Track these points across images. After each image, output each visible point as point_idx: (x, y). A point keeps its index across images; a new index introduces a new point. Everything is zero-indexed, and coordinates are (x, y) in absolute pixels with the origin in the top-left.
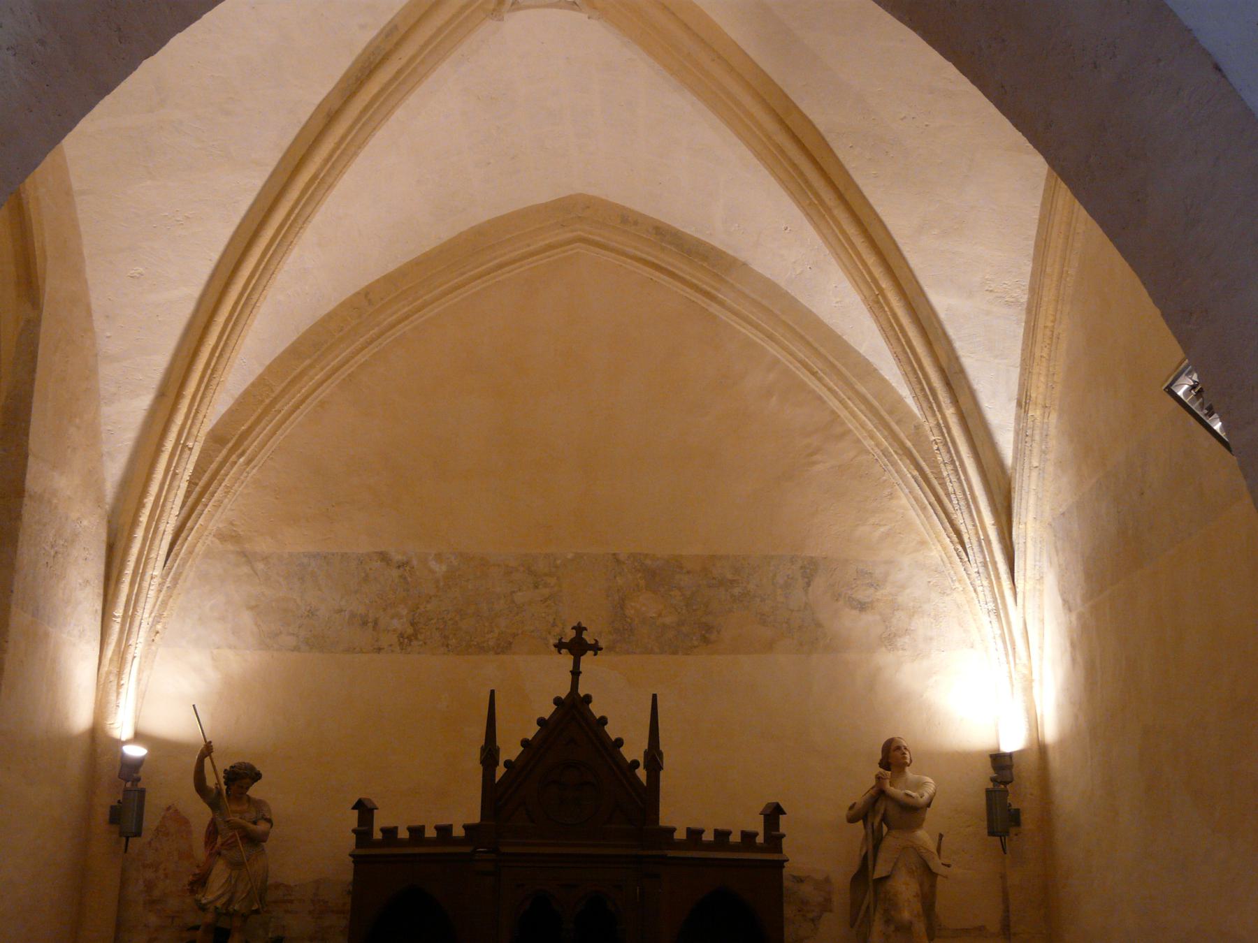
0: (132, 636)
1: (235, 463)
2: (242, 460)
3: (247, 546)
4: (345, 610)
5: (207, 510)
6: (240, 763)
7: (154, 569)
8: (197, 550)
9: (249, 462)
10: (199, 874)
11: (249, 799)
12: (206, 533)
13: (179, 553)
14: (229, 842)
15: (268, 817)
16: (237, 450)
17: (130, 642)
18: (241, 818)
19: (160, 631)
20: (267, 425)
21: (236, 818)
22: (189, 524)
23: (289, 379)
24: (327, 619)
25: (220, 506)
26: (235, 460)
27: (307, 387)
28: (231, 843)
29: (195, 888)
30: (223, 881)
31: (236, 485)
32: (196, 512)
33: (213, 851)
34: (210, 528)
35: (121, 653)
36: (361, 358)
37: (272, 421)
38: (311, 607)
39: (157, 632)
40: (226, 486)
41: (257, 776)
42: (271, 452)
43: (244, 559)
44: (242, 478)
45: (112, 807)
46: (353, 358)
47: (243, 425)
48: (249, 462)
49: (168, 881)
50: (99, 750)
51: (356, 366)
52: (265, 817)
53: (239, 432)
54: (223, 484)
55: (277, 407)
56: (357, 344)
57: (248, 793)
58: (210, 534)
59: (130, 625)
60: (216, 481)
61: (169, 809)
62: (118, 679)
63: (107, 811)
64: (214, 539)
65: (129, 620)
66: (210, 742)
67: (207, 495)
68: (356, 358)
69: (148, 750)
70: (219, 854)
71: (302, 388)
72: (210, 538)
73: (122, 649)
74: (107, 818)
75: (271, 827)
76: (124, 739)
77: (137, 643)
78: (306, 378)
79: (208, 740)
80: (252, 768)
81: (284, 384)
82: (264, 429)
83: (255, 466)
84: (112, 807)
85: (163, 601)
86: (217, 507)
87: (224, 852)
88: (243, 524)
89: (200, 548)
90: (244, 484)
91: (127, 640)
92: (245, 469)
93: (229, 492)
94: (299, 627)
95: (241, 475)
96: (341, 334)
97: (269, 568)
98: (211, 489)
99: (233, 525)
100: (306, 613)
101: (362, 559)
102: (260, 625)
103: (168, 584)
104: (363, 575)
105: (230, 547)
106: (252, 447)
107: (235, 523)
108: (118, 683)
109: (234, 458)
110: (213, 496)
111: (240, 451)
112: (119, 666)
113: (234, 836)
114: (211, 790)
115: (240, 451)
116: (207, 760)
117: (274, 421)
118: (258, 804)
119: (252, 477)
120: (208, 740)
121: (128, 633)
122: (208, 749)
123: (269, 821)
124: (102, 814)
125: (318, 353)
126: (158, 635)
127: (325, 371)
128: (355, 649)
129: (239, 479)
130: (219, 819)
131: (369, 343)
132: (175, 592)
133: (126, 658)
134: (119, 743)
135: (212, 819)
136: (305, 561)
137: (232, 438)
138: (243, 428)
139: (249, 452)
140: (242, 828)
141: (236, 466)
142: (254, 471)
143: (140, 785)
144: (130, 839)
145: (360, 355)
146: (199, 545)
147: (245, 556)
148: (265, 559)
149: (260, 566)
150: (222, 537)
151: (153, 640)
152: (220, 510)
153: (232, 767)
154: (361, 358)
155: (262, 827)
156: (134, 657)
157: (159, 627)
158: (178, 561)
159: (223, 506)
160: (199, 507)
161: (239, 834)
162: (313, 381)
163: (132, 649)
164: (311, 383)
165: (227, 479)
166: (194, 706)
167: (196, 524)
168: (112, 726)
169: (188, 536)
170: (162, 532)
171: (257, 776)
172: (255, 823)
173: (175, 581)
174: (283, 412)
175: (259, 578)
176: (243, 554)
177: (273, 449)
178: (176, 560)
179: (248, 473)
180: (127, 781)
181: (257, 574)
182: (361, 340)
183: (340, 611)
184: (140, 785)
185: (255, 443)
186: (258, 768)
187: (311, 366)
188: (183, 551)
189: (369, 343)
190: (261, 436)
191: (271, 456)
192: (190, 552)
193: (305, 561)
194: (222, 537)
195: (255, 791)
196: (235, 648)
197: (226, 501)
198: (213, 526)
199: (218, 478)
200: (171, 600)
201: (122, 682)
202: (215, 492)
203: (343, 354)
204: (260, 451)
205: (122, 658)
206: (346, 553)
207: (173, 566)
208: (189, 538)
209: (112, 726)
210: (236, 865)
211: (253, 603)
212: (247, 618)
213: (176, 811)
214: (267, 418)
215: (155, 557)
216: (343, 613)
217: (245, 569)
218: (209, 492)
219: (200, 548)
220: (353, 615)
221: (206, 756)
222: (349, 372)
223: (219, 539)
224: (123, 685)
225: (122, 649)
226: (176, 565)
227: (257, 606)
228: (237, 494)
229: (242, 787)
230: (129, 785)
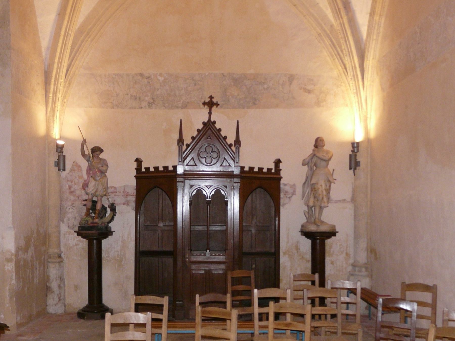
2: (89, 39)
32: (75, 59)
66: (85, 139)
67: (78, 53)
69: (65, 142)
79: (84, 138)
100: (115, 95)
103: (67, 85)
108: (53, 119)
109: (87, 39)
116: (85, 146)
120: (84, 138)
122: (85, 141)
134: (55, 140)
136: (114, 76)
151: (64, 105)
168: (52, 134)
170: (63, 65)
193: (114, 76)
195: (102, 156)
201: (54, 119)
207: (68, 78)
213: (76, 163)
215: (61, 75)
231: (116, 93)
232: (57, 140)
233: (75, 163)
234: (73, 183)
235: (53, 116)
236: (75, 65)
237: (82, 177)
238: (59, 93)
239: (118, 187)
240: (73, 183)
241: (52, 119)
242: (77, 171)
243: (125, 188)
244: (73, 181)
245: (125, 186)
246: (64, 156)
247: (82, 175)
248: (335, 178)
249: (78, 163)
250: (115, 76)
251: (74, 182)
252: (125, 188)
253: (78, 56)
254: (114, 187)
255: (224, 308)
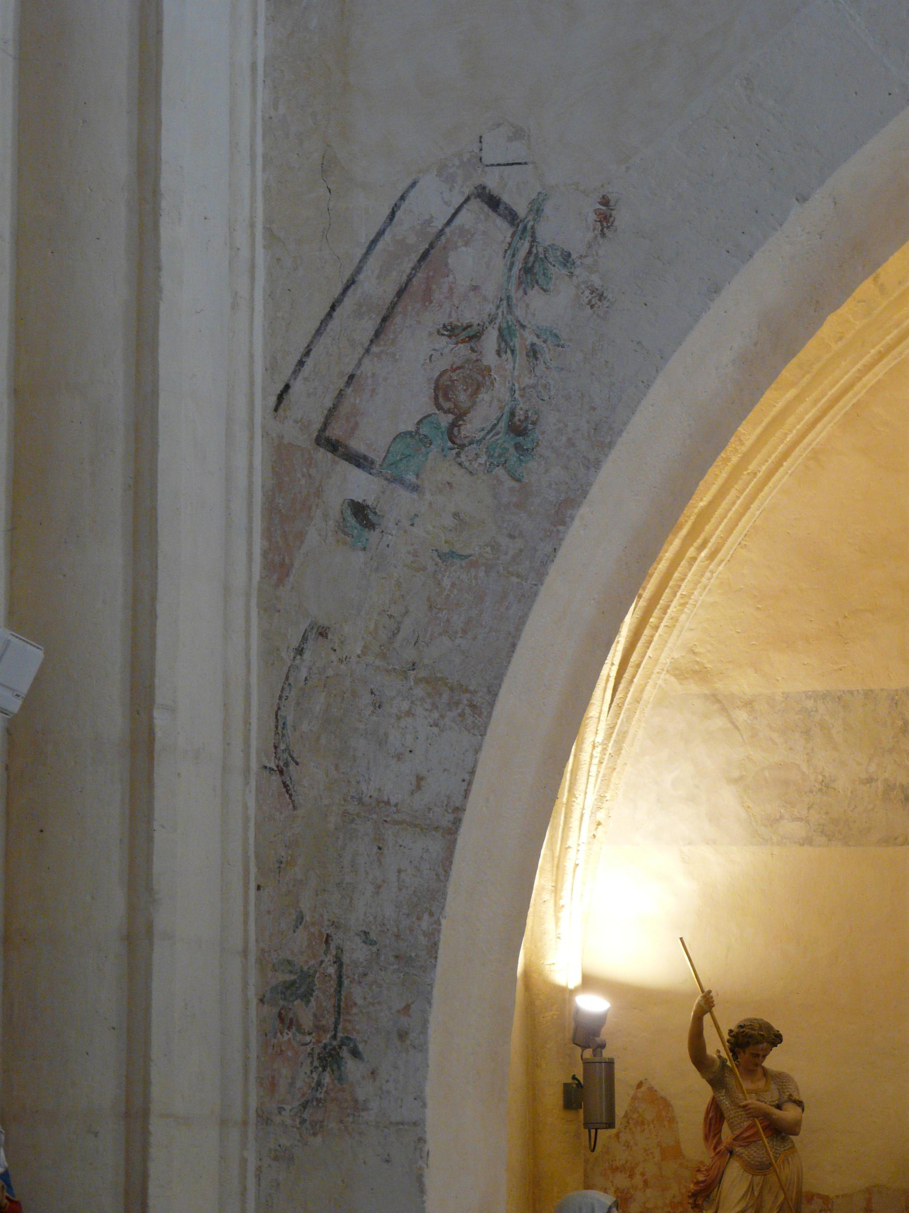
0: (571, 834)
1: (694, 559)
2: (703, 554)
3: (719, 685)
4: (877, 780)
5: (657, 635)
6: (750, 1020)
7: (597, 734)
8: (645, 696)
9: (712, 556)
10: (702, 1182)
11: (765, 1072)
12: (657, 670)
13: (623, 703)
14: (747, 1134)
15: (797, 1098)
16: (694, 541)
17: (569, 843)
18: (758, 1100)
19: (602, 821)
20: (738, 498)
21: (752, 1101)
22: (634, 658)
23: (766, 421)
24: (849, 794)
25: (674, 626)
26: (694, 554)
27: (794, 431)
28: (748, 1137)
29: (700, 1202)
30: (742, 1192)
31: (696, 593)
32: (643, 639)
33: (721, 1147)
34: (662, 660)
35: (556, 860)
36: (870, 379)
37: (744, 490)
38: (824, 776)
39: (599, 824)
40: (681, 594)
41: (776, 1039)
42: (742, 536)
43: (716, 707)
44: (704, 580)
45: (565, 1085)
46: (860, 379)
47: (701, 500)
48: (712, 556)
49: (648, 1191)
50: (538, 1003)
51: (864, 391)
52: (793, 1098)
53: (696, 511)
54: (678, 594)
55: (751, 468)
56: (866, 359)
57: (763, 1064)
58: (663, 669)
59: (565, 817)
60: (667, 591)
61: (640, 1085)
62: (556, 897)
63: (560, 1090)
64: (668, 676)
65: (563, 809)
66: (710, 992)
67: (657, 613)
68: (865, 380)
69: (611, 1004)
70: (731, 1153)
71: (786, 435)
72: (662, 676)
73: (557, 854)
74: (561, 1102)
75: (803, 1110)
76: (571, 986)
77: (579, 845)
78: (791, 420)
79: (706, 990)
80: (769, 1027)
81: (759, 430)
82: (734, 503)
83: (722, 561)
84: (565, 1085)
85: (604, 776)
86: (671, 628)
87: (738, 1149)
88: (709, 651)
89: (650, 693)
90: (707, 589)
91: (564, 839)
92: (707, 567)
93: (686, 603)
94: (809, 809)
95: (702, 576)
96: (840, 344)
97: (756, 718)
98: (661, 602)
99: (694, 653)
100: (818, 786)
101: (897, 697)
102: (749, 807)
103: (609, 750)
104: (900, 723)
105: (693, 688)
106: (718, 533)
107: (697, 650)
108: (556, 904)
109: (691, 552)
110: (665, 613)
111: (699, 541)
112: (554, 878)
113: (753, 1126)
114: (713, 1061)
115: (699, 541)
116: (707, 1018)
117: (747, 490)
118: (780, 1079)
119: (717, 578)
120: (706, 990)
121: (564, 829)
122: (707, 1004)
123: (800, 1104)
124: (553, 1097)
125: (808, 376)
126: (600, 827)
127: (819, 405)
128: (896, 839)
129: (699, 582)
130: (726, 1103)
131: (881, 356)
132: (620, 761)
133: (565, 866)
134: (564, 995)
135: (714, 1098)
136: (810, 704)
137: (686, 521)
138: (701, 504)
139: (713, 540)
140: (765, 1117)
141: (696, 564)
142: (721, 568)
143: (606, 1054)
144: (599, 1130)
145: (871, 374)
146: (648, 688)
147: (719, 701)
148: (749, 704)
149: (742, 716)
150: (680, 673)
151: (594, 836)
152: (675, 632)
153: (741, 1027)
154: (870, 379)
155: (790, 1113)
156: (577, 865)
157: (601, 816)
158: (622, 716)
159: (678, 625)
160: (647, 632)
161: (761, 1123)
162: (803, 422)
163: (571, 854)
164: (799, 427)
165: (684, 585)
166: (681, 939)
167: (643, 657)
168: (553, 967)
169: (634, 677)
170: (605, 678)
171: (776, 1039)
172: (779, 1107)
173: (619, 750)
174: (759, 475)
175: (742, 735)
176: (715, 698)
177: (745, 532)
178: (620, 714)
179: (712, 572)
180: (584, 1047)
181: (737, 728)
182: (873, 351)
183: (870, 780)
184: (606, 1054)
185: (721, 528)
186: (777, 1025)
187: (799, 399)
188: (628, 699)
189: (881, 356)
190: (729, 515)
191: (743, 543)
192: (637, 700)
193: (810, 704)
194: (680, 673)
195: (774, 1061)
196: (715, 843)
197: (683, 617)
198: (665, 659)
199: (671, 583)
200: (615, 774)
201: (561, 903)
202: (668, 606)
203: (846, 377)
204: (728, 537)
205: (558, 867)
206: (871, 691)
207: (616, 723)
208: (635, 680)
209: (553, 967)
210: (761, 1168)
211: (736, 774)
212: (728, 797)
213: (651, 1089)
214: (736, 486)
215: (597, 715)
216: (874, 784)
217: (719, 722)
218: (658, 607)
219: (650, 693)
220: (889, 787)
221: (706, 1012)
222: (855, 400)
223: (675, 676)
224: (563, 906)
225: (557, 854)
226: (619, 722)
227: (741, 778)
228: (698, 605)
229: (758, 1055)
230: (588, 1053)
231: (820, 778)
232: (573, 992)
233: (643, 1089)
234: (638, 1180)
235: (555, 887)
236: (642, 665)
237: (674, 1152)
238: (586, 793)
239: (837, 1196)
240: (638, 1180)
241: (551, 904)
242: (652, 1126)
243: (869, 1201)
244: (639, 1169)
245: (869, 1191)
246: (610, 1063)
247: (678, 1143)
248: (637, 1082)
249: (656, 1088)
250: (815, 701)
251: (643, 1174)
252: (869, 1201)
253: (656, 628)
254: (820, 1196)
255: (695, 562)
